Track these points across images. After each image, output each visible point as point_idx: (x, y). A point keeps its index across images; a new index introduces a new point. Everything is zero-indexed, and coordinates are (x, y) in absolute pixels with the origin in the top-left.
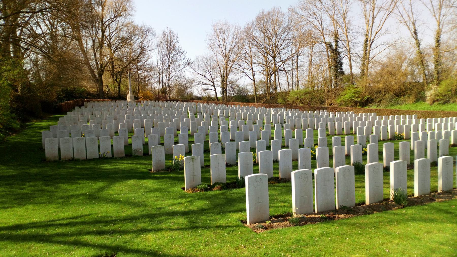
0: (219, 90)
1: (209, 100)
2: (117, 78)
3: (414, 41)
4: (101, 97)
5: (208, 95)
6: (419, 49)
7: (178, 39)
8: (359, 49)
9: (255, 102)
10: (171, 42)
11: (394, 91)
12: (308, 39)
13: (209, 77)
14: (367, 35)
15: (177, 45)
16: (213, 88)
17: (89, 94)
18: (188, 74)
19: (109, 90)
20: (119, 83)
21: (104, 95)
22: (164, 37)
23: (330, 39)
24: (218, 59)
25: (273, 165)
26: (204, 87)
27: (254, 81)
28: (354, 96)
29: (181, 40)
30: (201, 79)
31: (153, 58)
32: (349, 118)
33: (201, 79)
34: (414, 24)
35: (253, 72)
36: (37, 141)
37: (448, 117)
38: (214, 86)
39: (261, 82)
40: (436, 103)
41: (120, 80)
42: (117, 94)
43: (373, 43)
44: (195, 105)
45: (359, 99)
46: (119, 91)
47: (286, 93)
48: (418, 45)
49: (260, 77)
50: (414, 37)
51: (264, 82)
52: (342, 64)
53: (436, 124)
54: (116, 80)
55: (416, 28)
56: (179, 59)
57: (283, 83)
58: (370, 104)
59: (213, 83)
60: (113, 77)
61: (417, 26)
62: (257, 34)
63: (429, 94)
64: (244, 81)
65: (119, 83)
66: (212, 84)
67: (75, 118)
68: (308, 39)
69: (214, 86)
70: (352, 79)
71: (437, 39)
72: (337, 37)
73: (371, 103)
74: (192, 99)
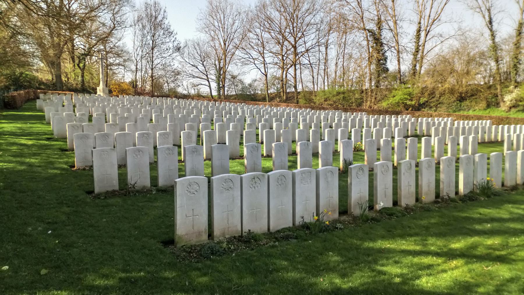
0: (214, 85)
1: (199, 96)
2: (80, 62)
4: (58, 89)
6: (494, 43)
7: (166, 14)
8: (407, 41)
10: (156, 18)
11: (462, 94)
12: (341, 24)
13: (201, 67)
16: (207, 83)
17: (41, 83)
19: (68, 79)
20: (83, 70)
21: (63, 86)
23: (372, 26)
24: (364, 16)
25: (118, 170)
26: (196, 81)
27: (266, 76)
28: (407, 99)
30: (189, 69)
33: (189, 69)
34: (489, 10)
36: (64, 145)
38: (208, 81)
40: (513, 110)
41: (84, 66)
42: (80, 86)
45: (413, 103)
48: (493, 36)
50: (488, 27)
51: (278, 79)
53: (515, 135)
54: (78, 65)
55: (492, 17)
56: (168, 40)
57: (305, 80)
58: (423, 110)
59: (207, 76)
60: (74, 62)
61: (492, 12)
63: (508, 98)
64: (250, 75)
65: (83, 70)
66: (206, 77)
68: (341, 24)
69: (208, 81)
70: (398, 77)
72: (379, 23)
73: (425, 108)
74: (174, 95)
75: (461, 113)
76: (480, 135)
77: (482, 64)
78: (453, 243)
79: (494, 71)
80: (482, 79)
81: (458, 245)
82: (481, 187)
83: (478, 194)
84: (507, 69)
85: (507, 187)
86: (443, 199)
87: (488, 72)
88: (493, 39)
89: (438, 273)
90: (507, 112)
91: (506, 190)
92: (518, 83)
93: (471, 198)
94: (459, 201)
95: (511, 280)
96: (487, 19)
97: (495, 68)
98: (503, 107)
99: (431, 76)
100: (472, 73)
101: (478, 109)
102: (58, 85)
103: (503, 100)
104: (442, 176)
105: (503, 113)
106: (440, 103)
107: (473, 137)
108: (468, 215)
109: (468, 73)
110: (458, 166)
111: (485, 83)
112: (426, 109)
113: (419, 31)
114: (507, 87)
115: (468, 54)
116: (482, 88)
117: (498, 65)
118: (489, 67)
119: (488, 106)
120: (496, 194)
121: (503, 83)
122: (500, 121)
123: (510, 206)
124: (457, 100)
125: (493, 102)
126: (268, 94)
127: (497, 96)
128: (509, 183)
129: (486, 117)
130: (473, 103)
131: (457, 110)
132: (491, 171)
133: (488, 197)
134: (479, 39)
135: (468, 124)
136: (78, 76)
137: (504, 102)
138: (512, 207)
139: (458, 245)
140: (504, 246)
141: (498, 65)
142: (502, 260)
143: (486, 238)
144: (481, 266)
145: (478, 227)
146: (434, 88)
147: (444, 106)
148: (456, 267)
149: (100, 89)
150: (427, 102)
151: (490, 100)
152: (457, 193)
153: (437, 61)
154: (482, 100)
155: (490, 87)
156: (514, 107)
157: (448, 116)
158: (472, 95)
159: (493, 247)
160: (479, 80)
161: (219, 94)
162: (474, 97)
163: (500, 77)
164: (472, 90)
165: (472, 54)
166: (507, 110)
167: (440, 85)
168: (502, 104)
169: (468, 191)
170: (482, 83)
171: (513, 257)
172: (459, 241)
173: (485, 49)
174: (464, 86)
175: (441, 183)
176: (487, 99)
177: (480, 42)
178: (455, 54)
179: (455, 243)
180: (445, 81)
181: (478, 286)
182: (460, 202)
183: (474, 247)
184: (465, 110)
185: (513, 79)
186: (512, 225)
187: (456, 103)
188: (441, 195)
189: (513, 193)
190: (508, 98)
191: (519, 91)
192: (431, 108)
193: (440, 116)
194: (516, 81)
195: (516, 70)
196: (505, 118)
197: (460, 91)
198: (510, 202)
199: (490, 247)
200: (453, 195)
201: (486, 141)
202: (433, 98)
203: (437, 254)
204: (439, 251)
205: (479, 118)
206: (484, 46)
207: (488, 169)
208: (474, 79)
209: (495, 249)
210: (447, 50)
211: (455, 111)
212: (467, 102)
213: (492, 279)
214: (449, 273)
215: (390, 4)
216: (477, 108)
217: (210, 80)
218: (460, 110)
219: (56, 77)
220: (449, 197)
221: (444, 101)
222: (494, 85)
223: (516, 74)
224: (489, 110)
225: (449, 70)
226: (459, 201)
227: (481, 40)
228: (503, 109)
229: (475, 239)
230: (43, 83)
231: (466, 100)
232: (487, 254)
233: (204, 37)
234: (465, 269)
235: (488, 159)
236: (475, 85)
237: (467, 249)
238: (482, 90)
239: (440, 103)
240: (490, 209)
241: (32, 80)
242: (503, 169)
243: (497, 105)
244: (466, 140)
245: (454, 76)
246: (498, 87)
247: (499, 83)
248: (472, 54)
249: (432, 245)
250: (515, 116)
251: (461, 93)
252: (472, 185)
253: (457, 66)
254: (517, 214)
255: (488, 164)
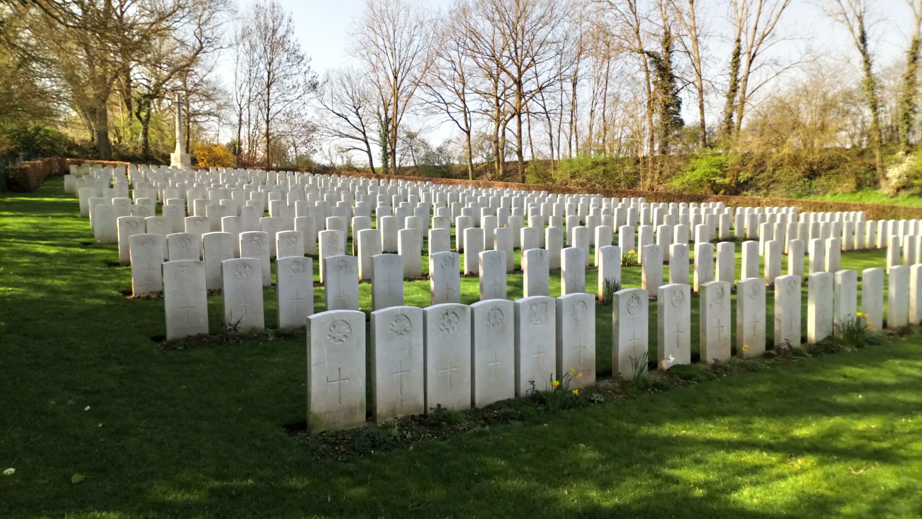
0: (377, 150)
1: (350, 170)
2: (140, 109)
3: (858, 57)
5: (349, 161)
6: (869, 75)
7: (291, 25)
8: (717, 73)
9: (468, 178)
12: (601, 43)
13: (354, 119)
14: (739, 41)
15: (292, 38)
17: (72, 145)
18: (311, 110)
19: (120, 139)
21: (111, 152)
22: (257, 17)
23: (654, 46)
26: (346, 142)
27: (468, 133)
28: (715, 174)
29: (297, 26)
31: (225, 70)
32: (603, 217)
34: (860, 18)
35: (465, 111)
37: (888, 219)
38: (367, 142)
39: (484, 137)
40: (903, 193)
41: (148, 116)
42: (140, 151)
43: (756, 58)
44: (314, 180)
45: (727, 181)
46: (146, 142)
47: (547, 163)
48: (868, 63)
49: (482, 126)
50: (859, 47)
51: (489, 138)
52: (678, 104)
54: (138, 115)
55: (866, 29)
57: (537, 141)
58: (745, 193)
59: (364, 133)
60: (130, 108)
62: (484, 26)
63: (894, 174)
64: (437, 130)
65: (146, 122)
66: (362, 136)
67: (911, 314)
68: (601, 43)
69: (367, 142)
70: (701, 134)
71: (912, 54)
73: (747, 190)
75: (812, 199)
76: (844, 238)
77: (847, 112)
78: (797, 427)
79: (869, 125)
80: (848, 140)
81: (805, 430)
82: (846, 328)
83: (841, 342)
84: (892, 121)
85: (891, 328)
86: (779, 350)
87: (859, 126)
88: (868, 69)
89: (771, 480)
90: (892, 197)
91: (891, 334)
92: (911, 146)
93: (829, 348)
94: (807, 354)
95: (900, 493)
96: (858, 34)
97: (871, 119)
98: (886, 189)
99: (758, 134)
100: (830, 128)
101: (842, 192)
102: (103, 150)
103: (884, 175)
104: (778, 310)
105: (884, 199)
106: (773, 182)
107: (833, 242)
108: (823, 378)
109: (823, 128)
110: (806, 293)
111: (854, 147)
112: (750, 191)
113: (737, 54)
114: (892, 153)
115: (824, 95)
116: (848, 155)
117: (876, 115)
118: (860, 117)
119: (859, 186)
120: (873, 341)
121: (884, 146)
122: (879, 213)
123: (897, 362)
124: (805, 177)
125: (868, 180)
126: (472, 165)
127: (875, 169)
128: (896, 322)
129: (855, 205)
130: (833, 182)
131: (804, 193)
132: (863, 302)
133: (859, 346)
134: (843, 69)
135: (823, 218)
136: (137, 134)
137: (887, 179)
138: (901, 365)
139: (805, 430)
140: (886, 432)
141: (876, 115)
142: (882, 457)
143: (854, 419)
144: (845, 468)
145: (841, 399)
146: (763, 155)
147: (781, 186)
148: (803, 471)
149: (176, 157)
150: (751, 179)
151: (861, 176)
152: (804, 339)
153: (769, 108)
154: (847, 176)
155: (862, 154)
156: (904, 187)
157: (789, 204)
158: (831, 168)
159: (867, 434)
160: (844, 140)
161: (385, 166)
162: (833, 171)
163: (880, 135)
164: (830, 158)
165: (830, 95)
166: (892, 194)
167: (774, 150)
168: (883, 183)
169: (823, 336)
170: (848, 146)
171: (902, 452)
172: (808, 424)
173: (854, 87)
174: (816, 152)
175: (776, 323)
176: (856, 174)
177: (844, 74)
178: (801, 96)
179: (801, 428)
180: (784, 142)
181: (841, 502)
182: (810, 356)
183: (834, 434)
184: (817, 193)
185: (902, 140)
186: (902, 396)
187: (802, 182)
188: (776, 343)
189: (903, 339)
190: (894, 174)
191: (913, 160)
192: (758, 189)
193: (773, 204)
194: (907, 143)
195: (907, 123)
196: (888, 207)
197: (810, 159)
198: (897, 356)
199: (861, 435)
200: (796, 343)
201: (856, 247)
202: (762, 172)
203: (769, 448)
204: (772, 441)
205: (843, 208)
206: (852, 81)
207: (859, 298)
208: (834, 139)
209: (870, 439)
210: (786, 89)
211: (800, 196)
212: (822, 180)
213: (865, 490)
214: (791, 480)
215: (686, 6)
216: (838, 189)
217: (369, 140)
218: (809, 194)
219: (99, 135)
220: (789, 346)
221: (782, 178)
222: (869, 150)
223: (908, 130)
224: (860, 193)
225: (791, 124)
226: (807, 354)
227: (846, 71)
228: (886, 192)
229: (836, 421)
230: (76, 146)
231: (820, 175)
232: (857, 448)
233: (359, 65)
234: (819, 472)
235: (859, 279)
236: (836, 149)
237: (822, 437)
238: (849, 159)
239: (773, 182)
240: (862, 368)
241: (57, 140)
242: (886, 298)
243: (875, 184)
244: (820, 246)
245: (798, 134)
246: (877, 153)
247: (877, 145)
248: (830, 95)
249: (761, 431)
250: (906, 204)
251: (811, 164)
252: (830, 325)
253: (805, 116)
254: (909, 376)
255: (859, 289)
